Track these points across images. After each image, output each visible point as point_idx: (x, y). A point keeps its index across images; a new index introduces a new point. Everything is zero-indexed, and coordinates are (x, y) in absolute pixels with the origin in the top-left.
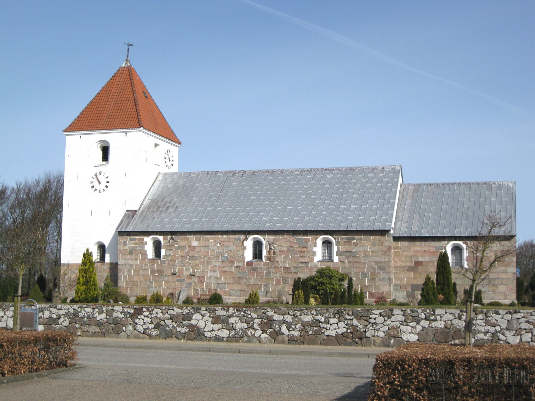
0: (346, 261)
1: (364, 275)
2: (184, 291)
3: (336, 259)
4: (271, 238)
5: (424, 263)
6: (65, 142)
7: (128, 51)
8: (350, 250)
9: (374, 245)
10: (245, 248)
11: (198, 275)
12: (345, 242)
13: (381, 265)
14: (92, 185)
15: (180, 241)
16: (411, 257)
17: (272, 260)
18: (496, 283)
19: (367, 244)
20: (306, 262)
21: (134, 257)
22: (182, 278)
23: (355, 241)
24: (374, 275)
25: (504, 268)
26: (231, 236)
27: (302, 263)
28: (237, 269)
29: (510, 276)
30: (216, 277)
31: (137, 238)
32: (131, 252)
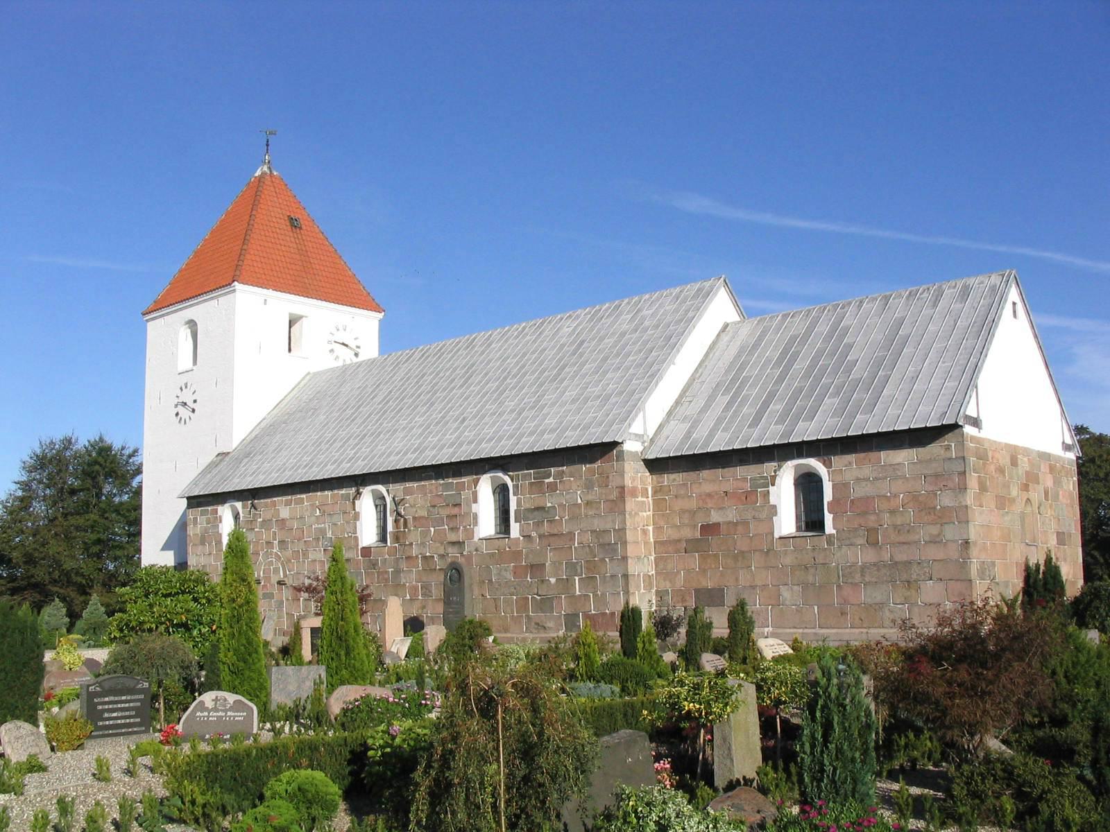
0: (534, 534)
1: (572, 567)
2: (270, 618)
4: (398, 488)
5: (723, 528)
8: (542, 505)
9: (589, 486)
10: (357, 517)
12: (531, 484)
13: (606, 540)
16: (693, 513)
18: (914, 577)
19: (574, 487)
20: (459, 542)
23: (551, 480)
24: (592, 566)
25: (934, 530)
26: (336, 492)
27: (453, 543)
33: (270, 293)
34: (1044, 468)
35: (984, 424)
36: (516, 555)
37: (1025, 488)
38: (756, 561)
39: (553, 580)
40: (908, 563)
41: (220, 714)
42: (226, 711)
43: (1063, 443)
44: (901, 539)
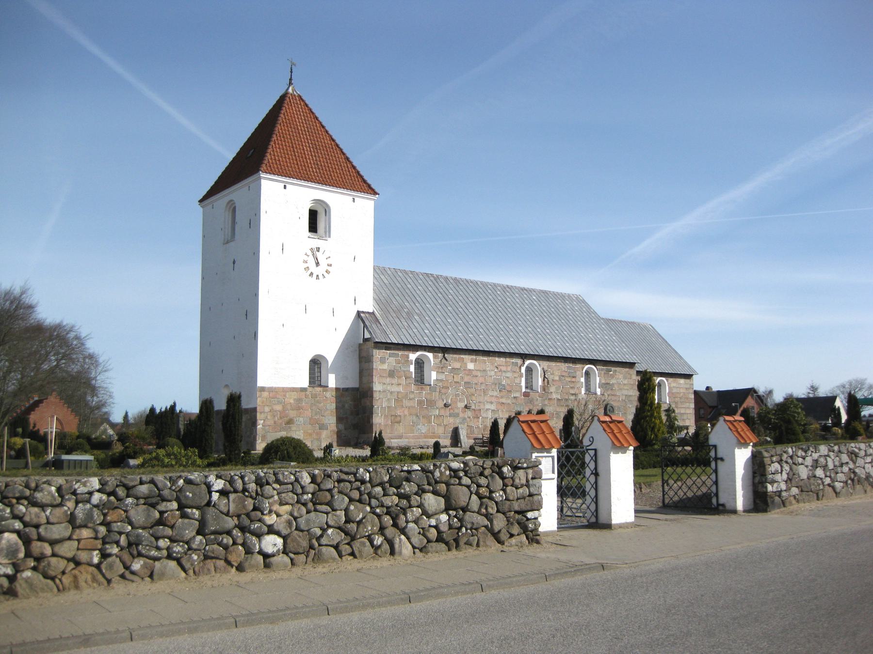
4: (545, 364)
6: (249, 139)
7: (291, 79)
9: (625, 378)
11: (473, 407)
14: (306, 265)
15: (454, 361)
21: (395, 381)
22: (456, 411)
26: (508, 359)
27: (573, 394)
28: (514, 401)
30: (493, 411)
31: (400, 353)
32: (391, 374)
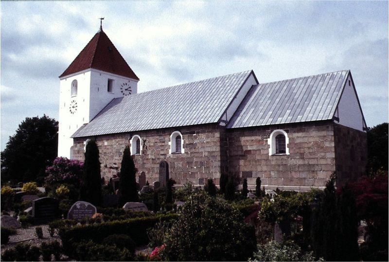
3: (183, 151)
5: (252, 152)
6: (117, 51)
13: (214, 154)
14: (121, 90)
17: (145, 153)
18: (316, 169)
19: (203, 137)
21: (79, 155)
25: (323, 154)
27: (162, 155)
29: (329, 162)
33: (102, 72)
34: (358, 136)
35: (340, 119)
36: (182, 159)
37: (352, 141)
38: (263, 162)
39: (195, 167)
40: (314, 165)
41: (83, 210)
42: (85, 209)
43: (363, 127)
44: (311, 157)
